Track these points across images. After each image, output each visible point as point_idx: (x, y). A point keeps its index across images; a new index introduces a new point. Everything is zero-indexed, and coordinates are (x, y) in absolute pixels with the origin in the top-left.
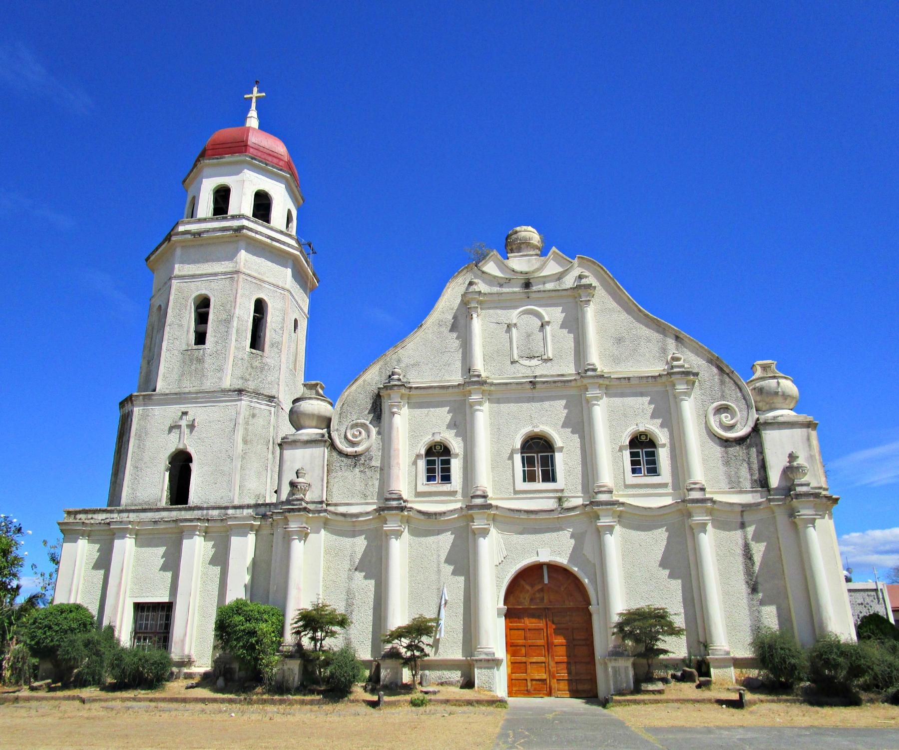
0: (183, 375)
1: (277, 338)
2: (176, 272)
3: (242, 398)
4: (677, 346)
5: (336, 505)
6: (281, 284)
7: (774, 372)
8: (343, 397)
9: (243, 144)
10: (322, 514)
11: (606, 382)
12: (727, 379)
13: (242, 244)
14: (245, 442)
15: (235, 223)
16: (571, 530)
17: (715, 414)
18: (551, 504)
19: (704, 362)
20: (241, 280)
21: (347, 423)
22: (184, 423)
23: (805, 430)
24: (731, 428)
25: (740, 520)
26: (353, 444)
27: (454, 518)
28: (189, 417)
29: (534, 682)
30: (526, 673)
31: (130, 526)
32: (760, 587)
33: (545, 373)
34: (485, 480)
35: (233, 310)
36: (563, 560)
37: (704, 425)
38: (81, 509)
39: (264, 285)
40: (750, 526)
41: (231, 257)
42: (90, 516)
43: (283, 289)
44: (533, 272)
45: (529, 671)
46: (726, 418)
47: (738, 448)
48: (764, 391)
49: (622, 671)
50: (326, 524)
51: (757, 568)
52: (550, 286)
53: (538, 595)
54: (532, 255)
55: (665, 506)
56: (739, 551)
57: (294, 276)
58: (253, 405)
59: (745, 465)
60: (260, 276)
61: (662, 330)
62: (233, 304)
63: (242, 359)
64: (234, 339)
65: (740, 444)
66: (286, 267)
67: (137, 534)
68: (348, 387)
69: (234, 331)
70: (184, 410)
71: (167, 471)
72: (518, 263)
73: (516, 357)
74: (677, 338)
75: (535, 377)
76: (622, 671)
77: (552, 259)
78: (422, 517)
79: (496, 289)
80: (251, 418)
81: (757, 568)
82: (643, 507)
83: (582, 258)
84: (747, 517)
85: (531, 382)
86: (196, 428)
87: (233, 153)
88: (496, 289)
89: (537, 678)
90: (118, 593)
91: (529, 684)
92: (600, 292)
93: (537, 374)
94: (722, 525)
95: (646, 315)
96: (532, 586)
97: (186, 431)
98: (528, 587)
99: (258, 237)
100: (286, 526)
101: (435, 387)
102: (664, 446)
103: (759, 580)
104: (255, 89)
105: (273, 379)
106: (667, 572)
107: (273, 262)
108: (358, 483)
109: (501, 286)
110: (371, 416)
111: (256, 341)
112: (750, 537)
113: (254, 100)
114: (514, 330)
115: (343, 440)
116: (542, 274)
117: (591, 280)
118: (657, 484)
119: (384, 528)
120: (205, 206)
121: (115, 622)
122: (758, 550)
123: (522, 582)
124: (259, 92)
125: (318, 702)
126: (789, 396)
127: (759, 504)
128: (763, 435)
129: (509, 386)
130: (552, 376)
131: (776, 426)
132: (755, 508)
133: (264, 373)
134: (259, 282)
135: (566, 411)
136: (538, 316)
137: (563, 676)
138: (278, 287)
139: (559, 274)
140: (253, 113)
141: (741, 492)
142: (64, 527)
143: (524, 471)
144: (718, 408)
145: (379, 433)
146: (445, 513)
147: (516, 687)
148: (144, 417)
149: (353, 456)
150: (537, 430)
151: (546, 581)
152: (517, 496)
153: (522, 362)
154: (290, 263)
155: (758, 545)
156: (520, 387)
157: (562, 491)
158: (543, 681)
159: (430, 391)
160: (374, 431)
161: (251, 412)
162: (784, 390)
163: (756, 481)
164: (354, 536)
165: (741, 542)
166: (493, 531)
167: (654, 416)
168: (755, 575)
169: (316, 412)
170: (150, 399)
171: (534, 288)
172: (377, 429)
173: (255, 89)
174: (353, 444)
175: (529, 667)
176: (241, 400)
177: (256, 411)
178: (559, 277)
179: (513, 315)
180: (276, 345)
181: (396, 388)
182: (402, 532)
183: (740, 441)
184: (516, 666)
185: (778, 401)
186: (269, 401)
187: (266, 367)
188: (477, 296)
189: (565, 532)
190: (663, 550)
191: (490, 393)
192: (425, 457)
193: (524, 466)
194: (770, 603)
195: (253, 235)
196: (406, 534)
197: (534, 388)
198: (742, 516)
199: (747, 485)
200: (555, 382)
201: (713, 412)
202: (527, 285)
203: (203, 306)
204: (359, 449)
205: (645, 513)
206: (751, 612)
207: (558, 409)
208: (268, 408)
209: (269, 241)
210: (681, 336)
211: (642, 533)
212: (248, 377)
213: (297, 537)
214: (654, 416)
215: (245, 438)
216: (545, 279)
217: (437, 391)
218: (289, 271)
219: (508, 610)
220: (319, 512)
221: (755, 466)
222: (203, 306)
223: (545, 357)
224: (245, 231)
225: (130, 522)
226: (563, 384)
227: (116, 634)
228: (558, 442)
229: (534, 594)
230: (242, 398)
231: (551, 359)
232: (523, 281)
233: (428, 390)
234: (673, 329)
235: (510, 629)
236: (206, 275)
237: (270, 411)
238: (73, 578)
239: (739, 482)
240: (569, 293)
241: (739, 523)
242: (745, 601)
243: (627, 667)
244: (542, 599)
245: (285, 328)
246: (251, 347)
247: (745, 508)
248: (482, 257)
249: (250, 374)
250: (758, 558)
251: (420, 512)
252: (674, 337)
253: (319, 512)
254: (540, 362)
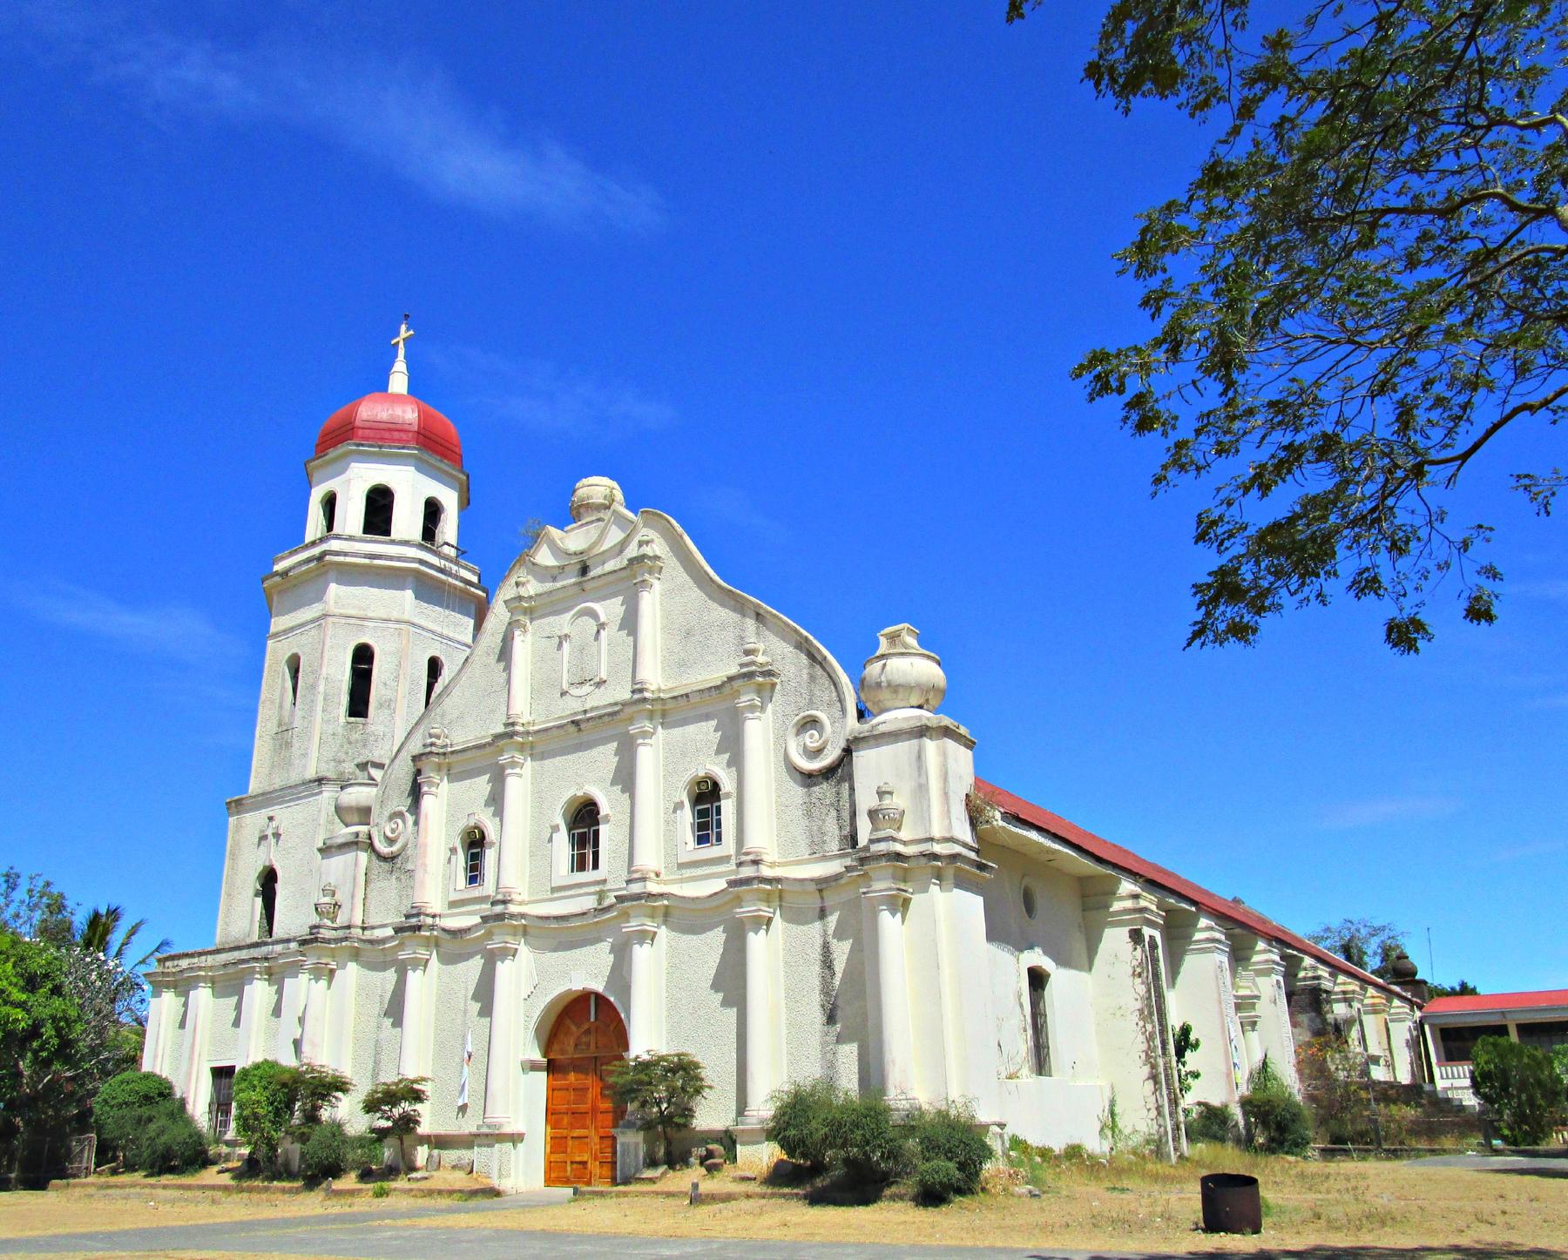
0: (273, 766)
1: (389, 694)
2: (273, 629)
4: (758, 628)
5: (373, 928)
6: (395, 615)
7: (906, 646)
9: (350, 427)
10: (344, 944)
11: (658, 707)
12: (819, 671)
13: (332, 575)
15: (316, 551)
16: (611, 940)
17: (797, 734)
18: (589, 903)
19: (791, 649)
20: (330, 626)
21: (387, 814)
22: (269, 832)
23: (915, 742)
24: (819, 752)
25: (818, 904)
26: (391, 842)
28: (274, 824)
29: (575, 1166)
30: (566, 1152)
31: (203, 973)
32: (839, 1013)
33: (595, 704)
34: (649, 857)
36: (598, 986)
37: (782, 759)
38: (193, 951)
39: (366, 623)
40: (831, 914)
41: (320, 596)
42: (176, 963)
43: (398, 621)
44: (590, 548)
45: (569, 1150)
46: (811, 739)
47: (825, 785)
48: (866, 683)
49: (632, 1149)
50: (356, 955)
51: (837, 981)
52: (610, 566)
53: (584, 1039)
54: (592, 522)
55: (716, 893)
56: (816, 954)
57: (419, 596)
59: (834, 813)
60: (361, 613)
61: (740, 607)
63: (334, 734)
64: (319, 709)
65: (827, 779)
67: (213, 981)
69: (321, 698)
70: (271, 814)
71: (256, 895)
72: (575, 539)
73: (565, 686)
74: (759, 617)
75: (585, 712)
76: (632, 1149)
77: (613, 523)
78: (448, 937)
79: (549, 586)
81: (837, 981)
82: (795, 880)
83: (646, 512)
84: (831, 899)
85: (573, 722)
87: (334, 445)
88: (549, 586)
89: (578, 1159)
90: (155, 1057)
91: (569, 1168)
92: (672, 565)
93: (588, 706)
94: (795, 917)
95: (719, 586)
96: (578, 1025)
97: (273, 841)
98: (574, 1028)
99: (348, 559)
102: (728, 795)
103: (840, 1002)
104: (403, 327)
105: (382, 752)
106: (720, 996)
109: (554, 579)
110: (409, 801)
111: (359, 704)
112: (830, 932)
113: (401, 345)
114: (566, 645)
115: (382, 838)
116: (602, 550)
117: (659, 547)
118: (717, 858)
120: (352, 514)
121: (189, 1091)
122: (842, 952)
123: (568, 1022)
124: (408, 330)
125: (297, 1191)
126: (899, 685)
127: (836, 877)
128: (854, 758)
129: (550, 733)
130: (605, 707)
131: (872, 742)
132: (834, 884)
133: (369, 747)
135: (617, 759)
136: (594, 615)
137: (607, 1157)
139: (619, 547)
140: (400, 366)
141: (825, 858)
142: (153, 979)
143: (573, 855)
144: (802, 723)
145: (416, 823)
146: (469, 929)
147: (554, 1176)
148: (239, 827)
150: (580, 794)
151: (592, 1019)
152: (556, 895)
153: (575, 691)
154: (410, 579)
155: (840, 943)
156: (562, 732)
157: (605, 881)
158: (584, 1163)
159: (469, 755)
160: (410, 819)
162: (890, 677)
163: (845, 837)
164: (384, 969)
165: (819, 942)
166: (524, 950)
167: (718, 752)
168: (834, 993)
169: (353, 804)
170: (241, 805)
171: (592, 574)
172: (414, 817)
173: (403, 327)
174: (391, 842)
175: (570, 1142)
176: (321, 792)
178: (622, 546)
179: (563, 623)
180: (388, 704)
181: (424, 758)
182: (427, 960)
183: (828, 773)
184: (557, 1144)
185: (885, 695)
188: (518, 604)
189: (605, 943)
190: (718, 961)
191: (532, 746)
192: (569, 830)
193: (573, 850)
194: (849, 1040)
195: (341, 559)
196: (778, 921)
198: (822, 898)
199: (833, 846)
200: (600, 717)
201: (794, 730)
202: (584, 570)
203: (294, 666)
204: (395, 848)
205: (693, 906)
206: (824, 1054)
207: (605, 756)
209: (367, 561)
210: (761, 612)
211: (695, 937)
212: (344, 757)
213: (885, 907)
214: (718, 752)
216: (604, 557)
218: (409, 594)
219: (549, 1061)
220: (346, 939)
221: (846, 815)
222: (294, 666)
223: (597, 680)
224: (328, 558)
225: (200, 968)
226: (611, 718)
227: (190, 1107)
228: (604, 809)
229: (579, 1037)
231: (605, 682)
232: (579, 566)
233: (464, 754)
234: (752, 602)
235: (553, 1090)
236: (284, 631)
238: (158, 1039)
239: (824, 842)
240: (623, 574)
241: (818, 909)
242: (818, 1035)
243: (637, 1144)
244: (588, 1045)
245: (402, 677)
247: (822, 884)
248: (534, 540)
249: (347, 753)
250: (839, 966)
251: (444, 930)
252: (754, 616)
253: (346, 939)
254: (593, 688)
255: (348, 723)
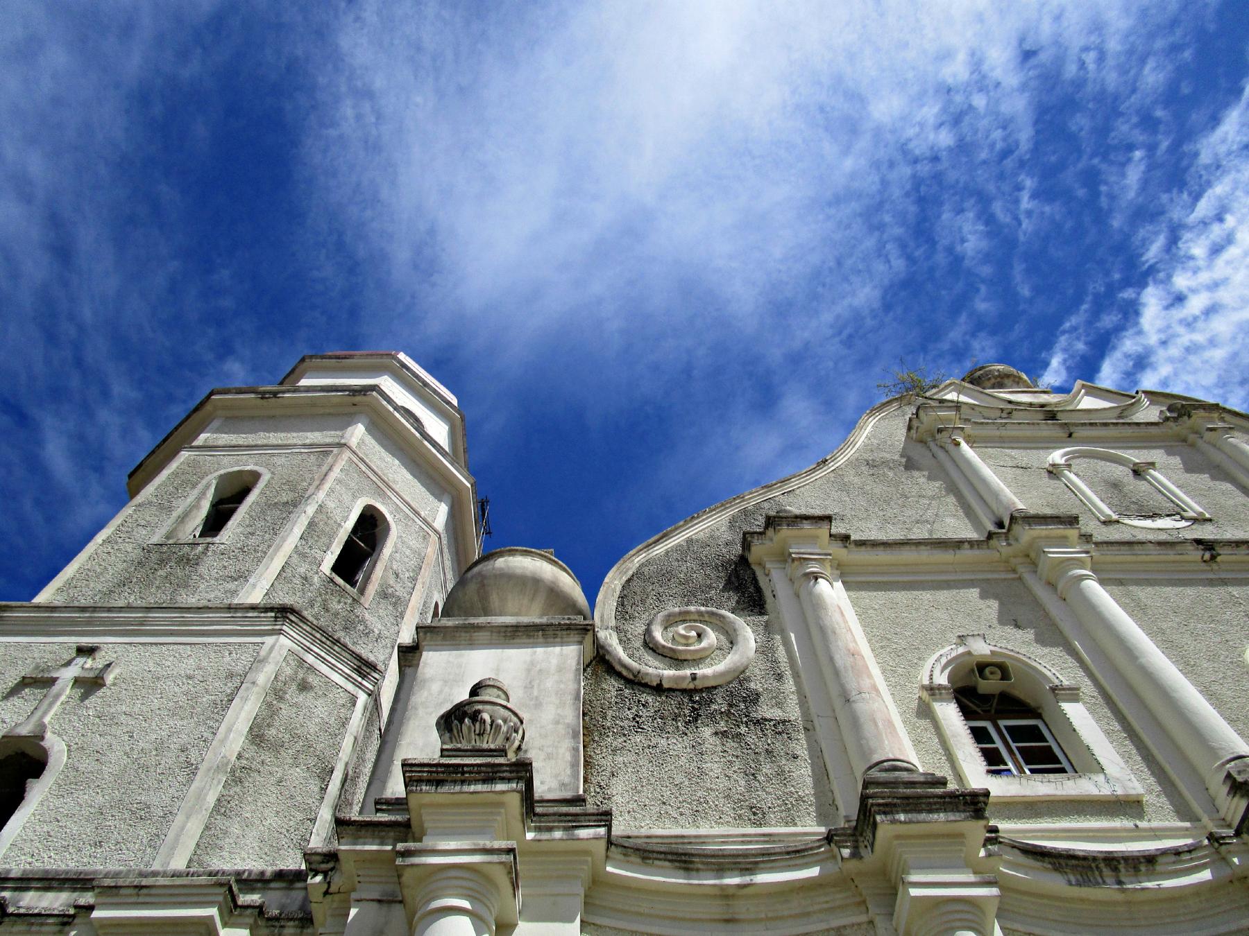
3: (284, 628)
8: (628, 564)
14: (257, 736)
27: (1198, 889)
35: (311, 489)
58: (310, 659)
62: (316, 483)
66: (440, 501)
68: (640, 547)
80: (294, 687)
86: (104, 690)
100: (411, 845)
101: (918, 543)
107: (414, 476)
108: (714, 767)
119: (914, 892)
134: (382, 486)
138: (417, 513)
149: (683, 691)
161: (300, 676)
176: (280, 632)
177: (311, 679)
186: (358, 671)
187: (361, 628)
197: (1213, 558)
208: (350, 687)
213: (466, 904)
215: (260, 727)
217: (924, 555)
230: (284, 628)
237: (353, 700)
246: (335, 569)
255: (332, 580)
